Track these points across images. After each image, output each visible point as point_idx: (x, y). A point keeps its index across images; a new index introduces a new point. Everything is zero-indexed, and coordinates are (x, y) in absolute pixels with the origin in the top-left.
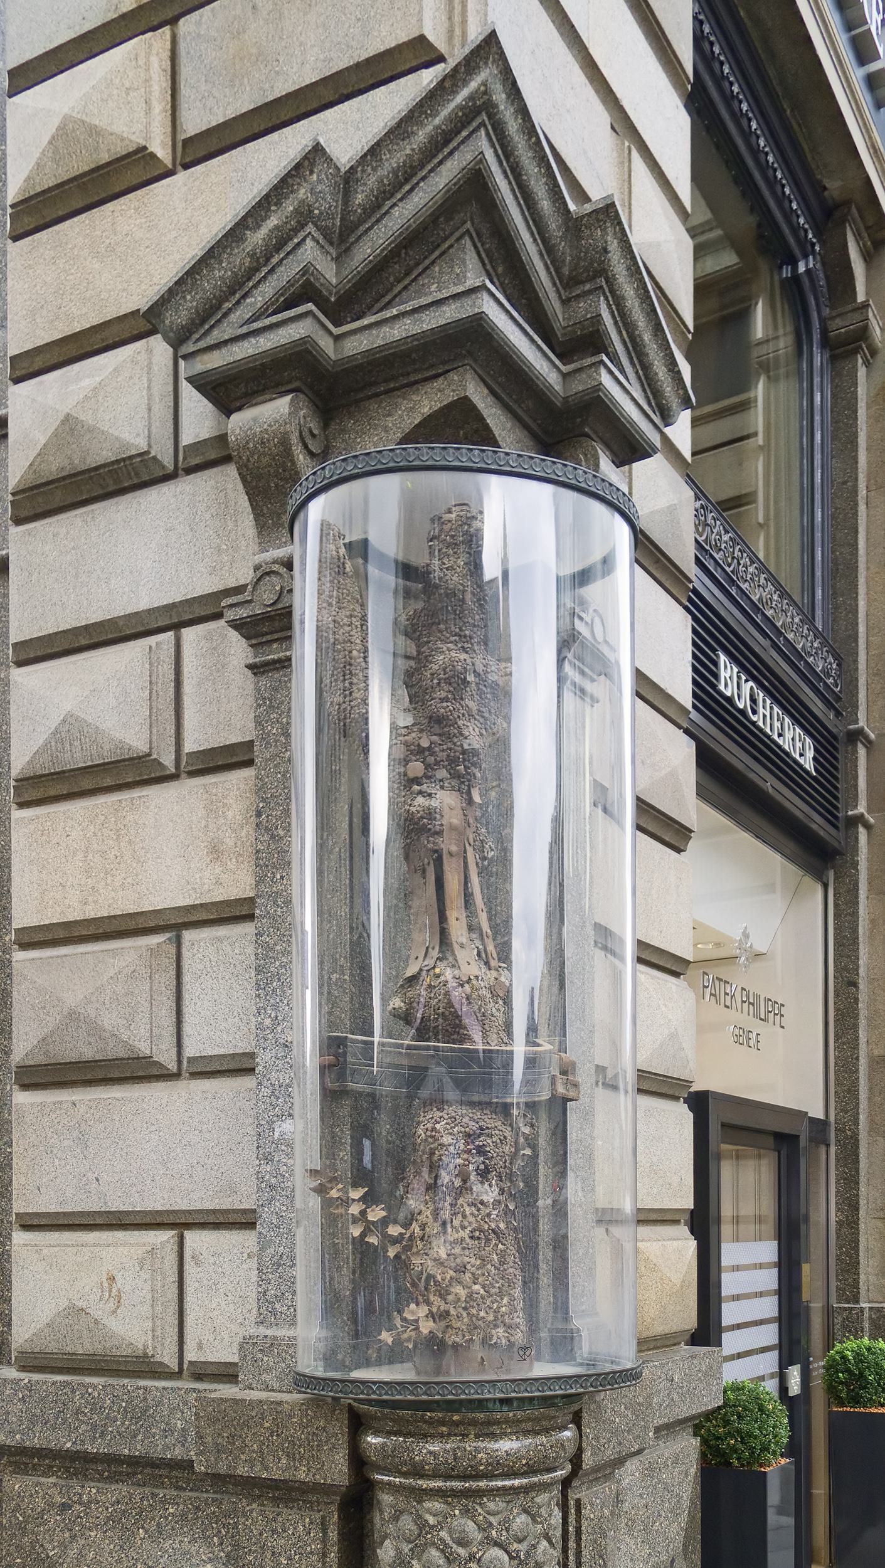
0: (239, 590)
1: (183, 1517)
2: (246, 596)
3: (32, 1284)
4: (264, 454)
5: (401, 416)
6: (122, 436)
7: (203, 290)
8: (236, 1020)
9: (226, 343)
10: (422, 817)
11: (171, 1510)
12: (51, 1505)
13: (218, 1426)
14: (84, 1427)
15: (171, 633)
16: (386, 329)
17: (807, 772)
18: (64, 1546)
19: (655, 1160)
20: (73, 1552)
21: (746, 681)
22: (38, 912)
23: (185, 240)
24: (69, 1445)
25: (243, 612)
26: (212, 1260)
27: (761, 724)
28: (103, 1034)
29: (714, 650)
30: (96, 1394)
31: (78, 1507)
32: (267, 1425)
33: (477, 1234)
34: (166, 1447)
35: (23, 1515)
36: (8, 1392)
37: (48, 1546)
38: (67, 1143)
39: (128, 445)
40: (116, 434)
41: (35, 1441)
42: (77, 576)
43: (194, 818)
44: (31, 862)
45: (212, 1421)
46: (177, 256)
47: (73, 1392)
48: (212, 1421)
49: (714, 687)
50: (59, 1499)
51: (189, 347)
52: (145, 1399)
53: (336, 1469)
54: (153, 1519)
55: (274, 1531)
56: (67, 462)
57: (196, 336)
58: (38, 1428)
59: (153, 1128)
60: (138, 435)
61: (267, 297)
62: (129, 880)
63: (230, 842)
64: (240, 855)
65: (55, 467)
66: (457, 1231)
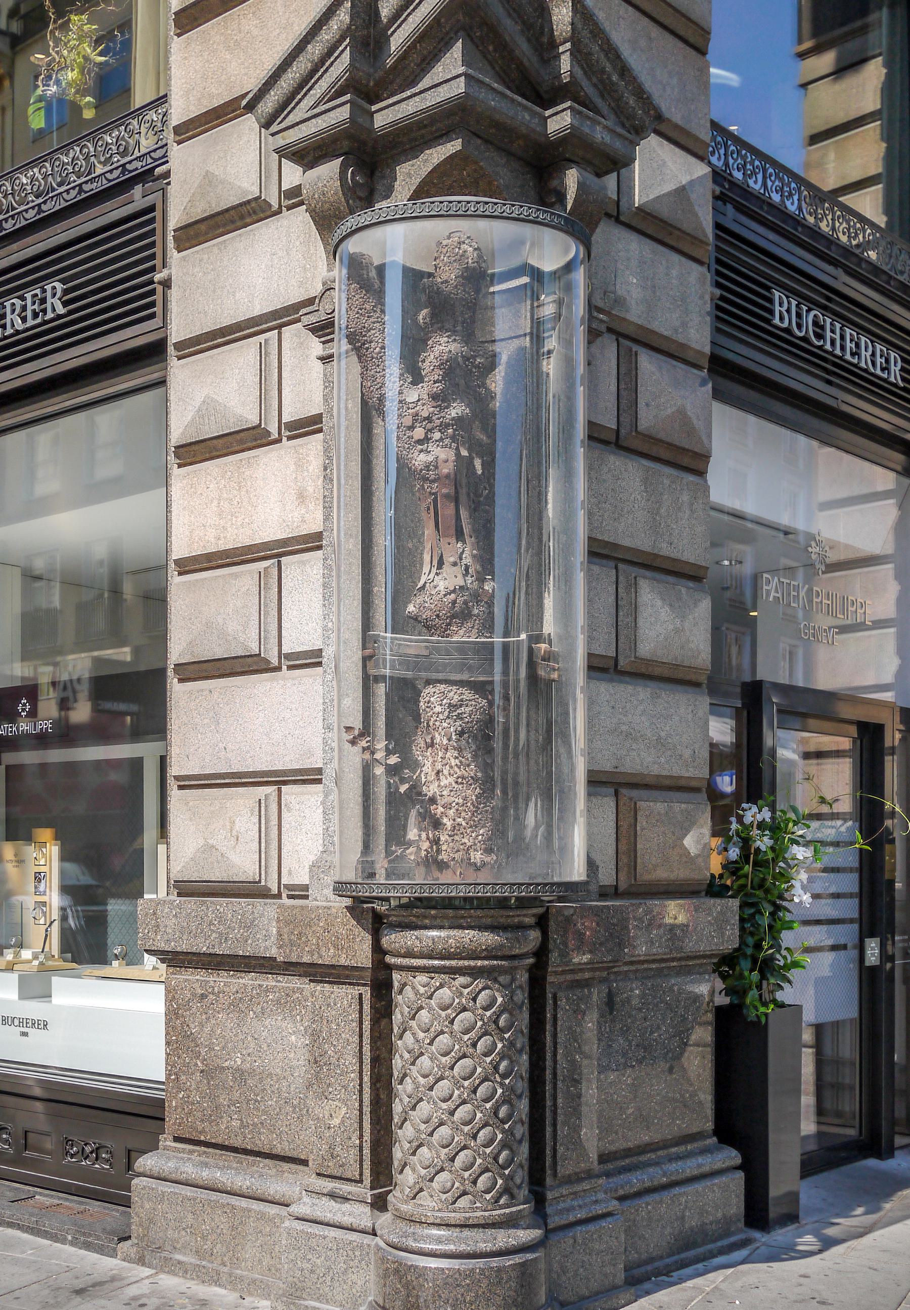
0: (310, 301)
1: (278, 1002)
2: (315, 307)
3: (182, 829)
4: (326, 202)
5: (419, 166)
6: (243, 185)
7: (282, 87)
8: (314, 624)
9: (297, 124)
10: (421, 470)
11: (271, 997)
12: (194, 995)
13: (291, 926)
14: (214, 935)
15: (276, 331)
16: (403, 105)
17: (895, 385)
18: (201, 1025)
19: (663, 734)
20: (207, 1029)
21: (808, 311)
22: (189, 546)
23: (284, 36)
24: (204, 949)
25: (313, 319)
26: (298, 808)
27: (828, 347)
28: (228, 638)
29: (768, 289)
30: (222, 910)
31: (211, 996)
32: (321, 924)
33: (460, 780)
34: (266, 948)
35: (177, 1003)
36: (166, 910)
37: (192, 1026)
38: (206, 721)
39: (246, 192)
40: (238, 183)
41: (183, 947)
42: (214, 291)
43: (288, 472)
44: (184, 509)
45: (287, 923)
46: (279, 48)
47: (208, 909)
48: (287, 923)
49: (768, 321)
50: (200, 991)
51: (274, 128)
52: (253, 912)
53: (360, 953)
54: (259, 1004)
55: (329, 1005)
56: (208, 205)
57: (279, 119)
58: (185, 937)
59: (261, 708)
60: (253, 184)
61: (324, 89)
62: (247, 520)
63: (311, 489)
64: (318, 499)
65: (199, 212)
66: (446, 778)
